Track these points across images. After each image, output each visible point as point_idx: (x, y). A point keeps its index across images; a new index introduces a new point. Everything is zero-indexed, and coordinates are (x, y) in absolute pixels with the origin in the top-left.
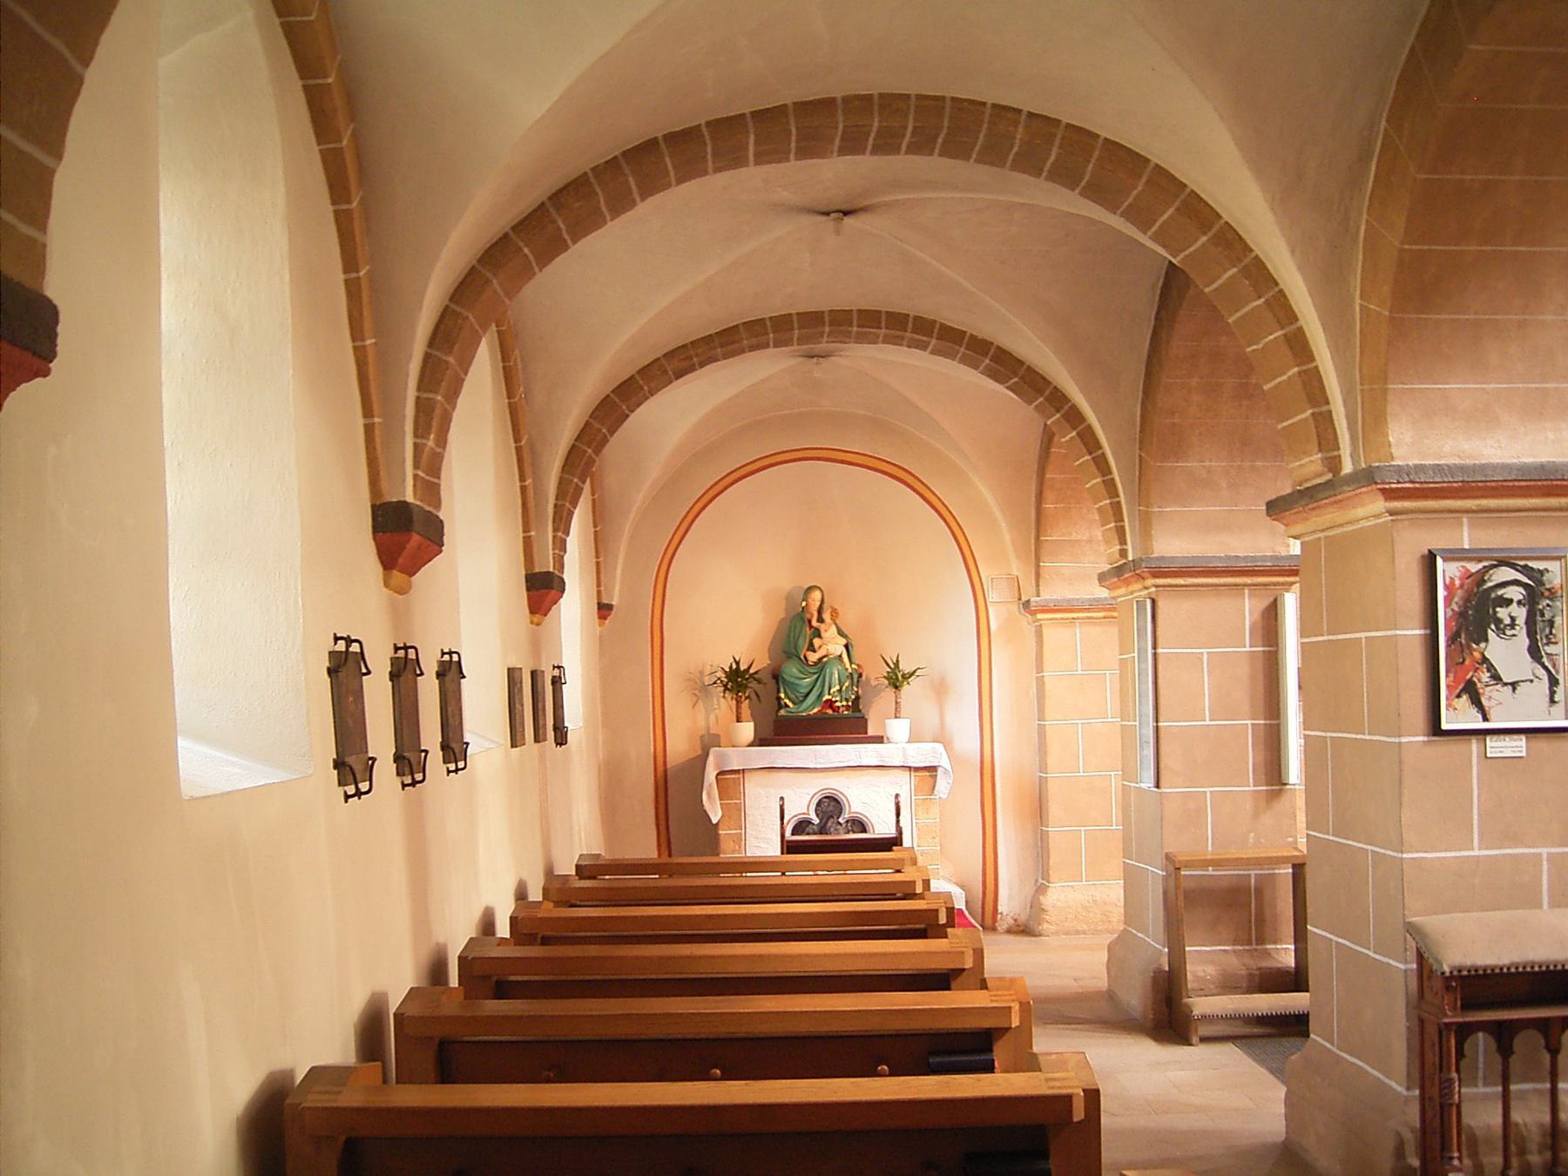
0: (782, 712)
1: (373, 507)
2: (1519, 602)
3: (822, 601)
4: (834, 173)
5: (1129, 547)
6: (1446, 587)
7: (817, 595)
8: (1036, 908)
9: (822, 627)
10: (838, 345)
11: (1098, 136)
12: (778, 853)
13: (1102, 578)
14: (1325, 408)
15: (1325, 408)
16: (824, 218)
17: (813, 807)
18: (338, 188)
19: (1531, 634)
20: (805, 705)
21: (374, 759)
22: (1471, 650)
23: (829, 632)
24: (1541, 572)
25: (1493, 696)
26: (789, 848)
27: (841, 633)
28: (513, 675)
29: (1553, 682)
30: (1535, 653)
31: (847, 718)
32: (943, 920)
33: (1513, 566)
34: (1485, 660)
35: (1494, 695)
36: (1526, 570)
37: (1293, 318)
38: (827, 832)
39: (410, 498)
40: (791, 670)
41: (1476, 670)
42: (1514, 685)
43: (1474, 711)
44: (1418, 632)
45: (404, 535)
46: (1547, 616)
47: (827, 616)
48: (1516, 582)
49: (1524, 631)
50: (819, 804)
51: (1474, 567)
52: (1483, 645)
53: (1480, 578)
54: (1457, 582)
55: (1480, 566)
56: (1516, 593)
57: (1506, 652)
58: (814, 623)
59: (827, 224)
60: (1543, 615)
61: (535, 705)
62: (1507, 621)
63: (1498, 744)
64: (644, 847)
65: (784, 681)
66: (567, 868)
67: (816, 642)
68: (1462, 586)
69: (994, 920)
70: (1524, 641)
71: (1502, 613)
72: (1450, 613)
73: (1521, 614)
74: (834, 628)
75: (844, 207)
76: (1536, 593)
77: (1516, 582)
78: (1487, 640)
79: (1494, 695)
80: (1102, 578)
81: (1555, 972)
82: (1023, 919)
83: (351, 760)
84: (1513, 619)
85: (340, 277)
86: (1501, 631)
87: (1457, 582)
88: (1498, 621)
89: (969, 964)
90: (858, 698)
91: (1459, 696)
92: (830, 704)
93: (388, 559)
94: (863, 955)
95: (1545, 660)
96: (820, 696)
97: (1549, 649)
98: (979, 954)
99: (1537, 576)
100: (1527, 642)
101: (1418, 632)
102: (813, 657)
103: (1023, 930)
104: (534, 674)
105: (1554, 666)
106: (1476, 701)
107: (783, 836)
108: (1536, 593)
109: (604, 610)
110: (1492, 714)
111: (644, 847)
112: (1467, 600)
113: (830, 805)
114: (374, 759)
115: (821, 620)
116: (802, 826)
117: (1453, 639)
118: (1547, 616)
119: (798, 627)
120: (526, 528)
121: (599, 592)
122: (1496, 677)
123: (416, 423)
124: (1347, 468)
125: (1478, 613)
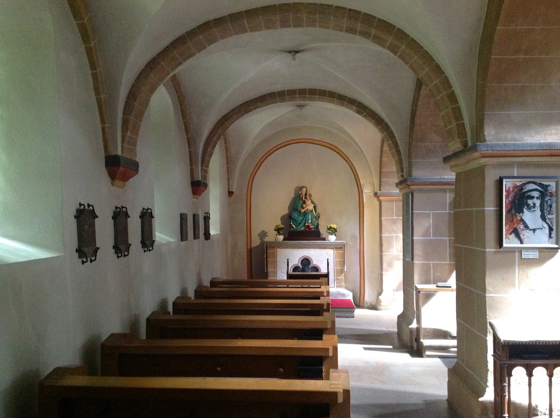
0: (292, 229)
1: (105, 157)
2: (537, 198)
3: (306, 191)
4: (290, 36)
5: (405, 174)
6: (506, 191)
7: (304, 189)
8: (378, 301)
9: (306, 200)
10: (309, 102)
11: (376, 17)
12: (286, 278)
13: (397, 185)
14: (462, 122)
15: (462, 122)
16: (289, 54)
17: (300, 262)
18: (85, 37)
19: (542, 210)
20: (299, 227)
21: (98, 248)
22: (516, 216)
23: (309, 202)
24: (547, 186)
25: (525, 234)
26: (290, 276)
27: (313, 202)
28: (183, 218)
29: (551, 229)
30: (543, 218)
31: (314, 232)
32: (325, 307)
33: (534, 183)
34: (522, 220)
35: (526, 234)
36: (540, 185)
37: (450, 87)
38: (306, 272)
39: (119, 153)
40: (295, 215)
41: (518, 224)
42: (534, 230)
43: (517, 240)
44: (493, 209)
45: (119, 168)
46: (549, 203)
47: (308, 197)
48: (536, 190)
49: (539, 209)
50: (302, 261)
51: (518, 183)
52: (521, 214)
53: (521, 188)
54: (511, 189)
55: (521, 183)
56: (536, 194)
57: (531, 217)
58: (304, 199)
59: (290, 56)
60: (547, 203)
61: (192, 227)
62: (532, 205)
63: (527, 253)
64: (243, 276)
65: (293, 219)
66: (206, 283)
67: (304, 205)
68: (513, 191)
69: (363, 303)
70: (538, 213)
71: (530, 202)
72: (508, 201)
73: (538, 202)
74: (310, 201)
75: (296, 50)
76: (544, 192)
77: (536, 190)
78: (523, 212)
79: (526, 234)
80: (397, 185)
81: (536, 345)
82: (373, 303)
83: (85, 250)
84: (534, 204)
85: (90, 72)
86: (529, 208)
87: (511, 189)
88: (528, 205)
89: (329, 326)
90: (318, 225)
91: (511, 234)
92: (308, 227)
93: (113, 176)
94: (294, 322)
95: (547, 220)
96: (305, 223)
97: (549, 216)
98: (333, 323)
99: (545, 187)
100: (540, 213)
101: (493, 209)
102: (303, 211)
103: (374, 307)
104: (194, 216)
105: (551, 223)
106: (518, 236)
107: (287, 272)
108: (544, 192)
109: (230, 193)
110: (525, 241)
111: (243, 276)
112: (515, 197)
113: (306, 261)
114: (98, 248)
115: (306, 198)
116: (296, 269)
117: (508, 212)
118: (549, 203)
119: (299, 199)
120: (191, 165)
121: (229, 188)
122: (526, 227)
123: (122, 127)
124: (470, 144)
125: (520, 201)
